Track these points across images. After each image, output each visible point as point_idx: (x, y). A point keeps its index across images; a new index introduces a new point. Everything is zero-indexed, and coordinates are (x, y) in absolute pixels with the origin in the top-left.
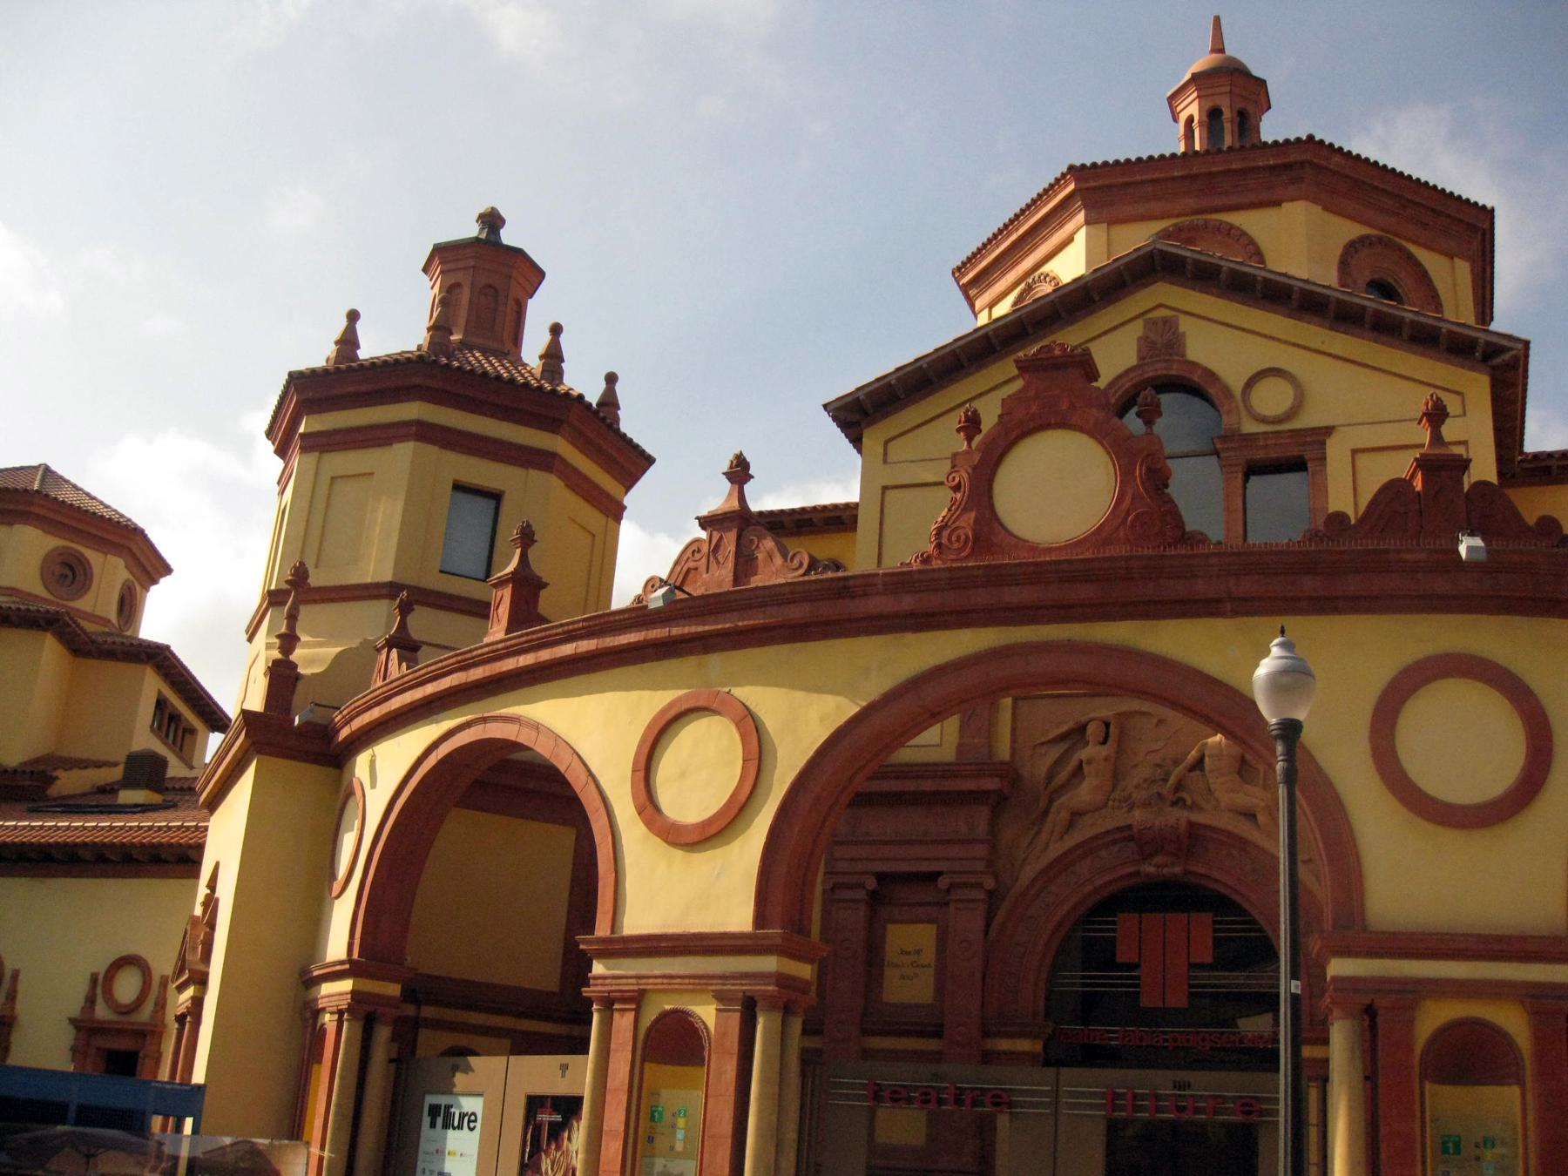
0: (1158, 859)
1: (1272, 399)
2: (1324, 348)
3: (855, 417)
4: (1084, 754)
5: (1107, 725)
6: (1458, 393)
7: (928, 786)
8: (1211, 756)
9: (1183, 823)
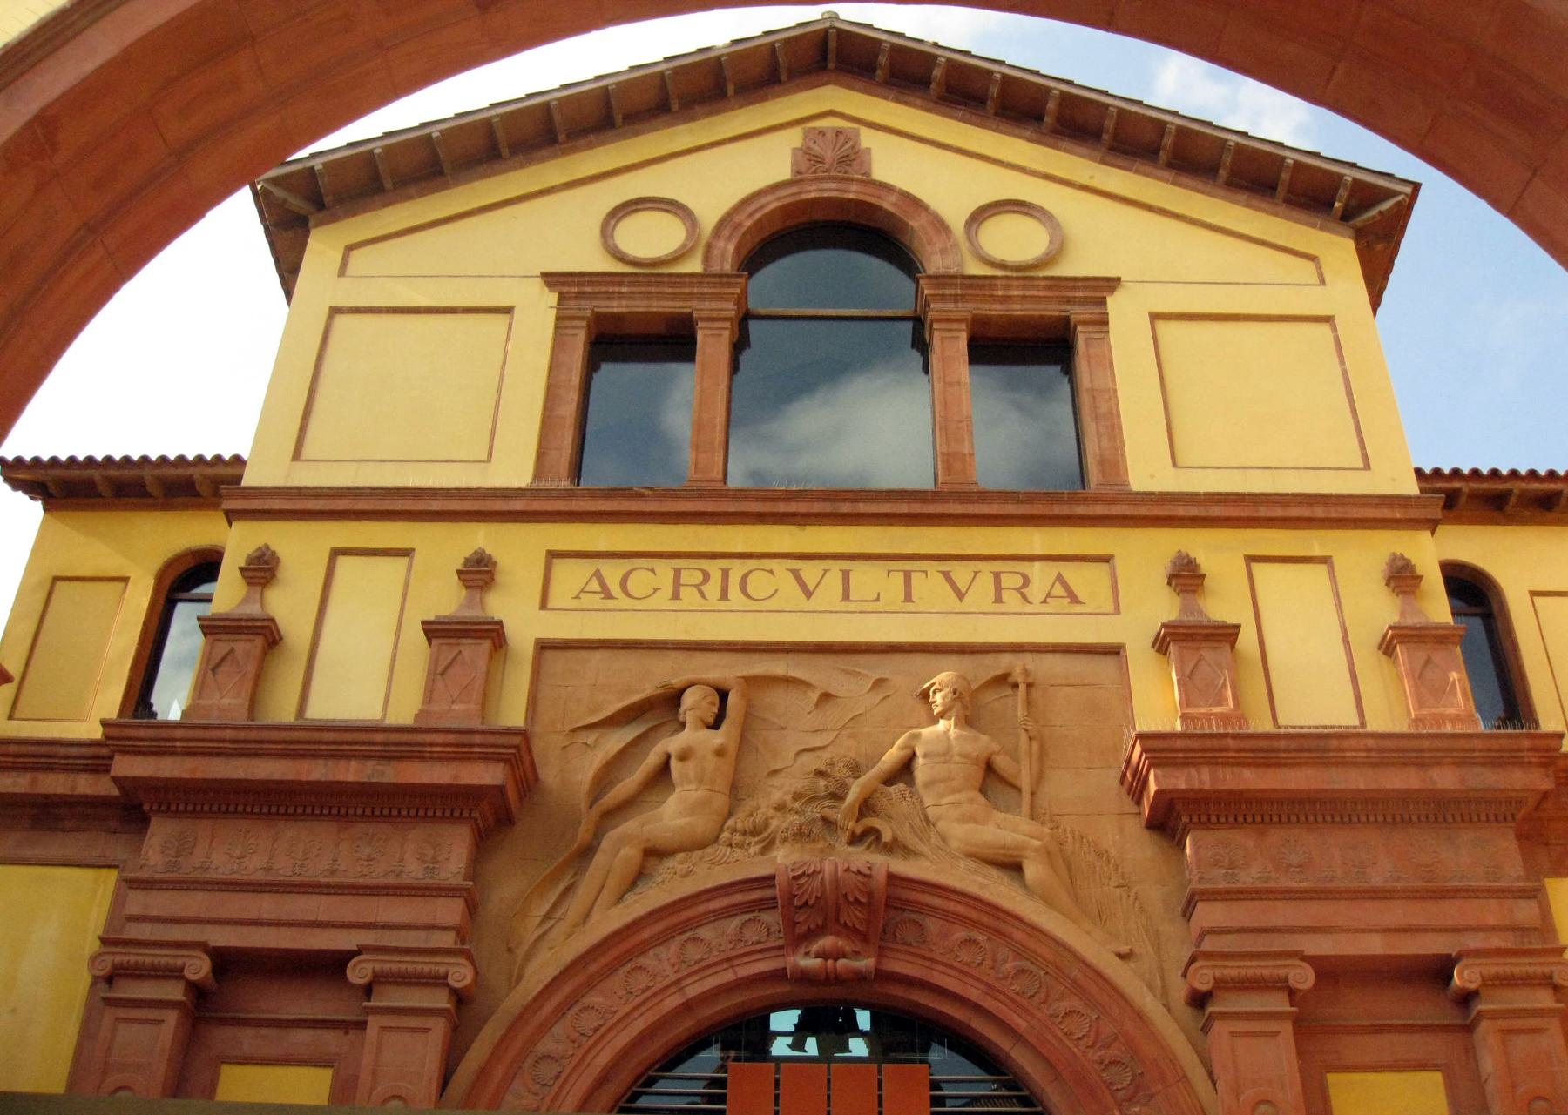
0: (827, 942)
1: (1015, 242)
2: (1095, 183)
3: (296, 203)
4: (673, 743)
5: (723, 695)
6: (1312, 258)
7: (350, 772)
8: (925, 756)
9: (880, 878)
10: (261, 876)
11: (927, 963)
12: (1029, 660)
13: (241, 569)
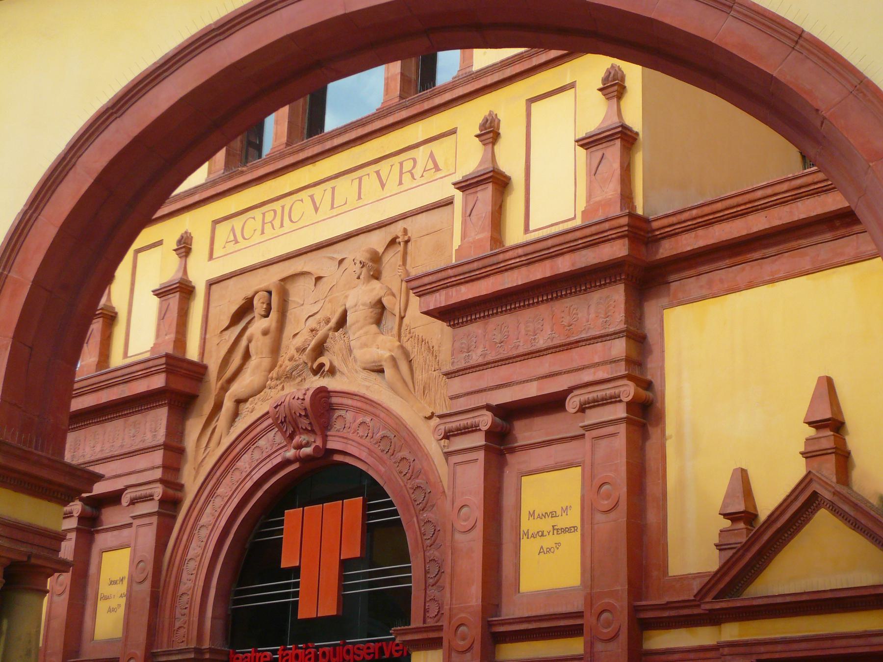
10: (481, 360)
11: (345, 441)
12: (401, 225)
13: (600, 90)
